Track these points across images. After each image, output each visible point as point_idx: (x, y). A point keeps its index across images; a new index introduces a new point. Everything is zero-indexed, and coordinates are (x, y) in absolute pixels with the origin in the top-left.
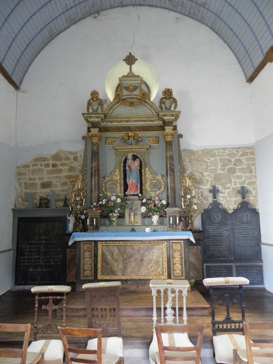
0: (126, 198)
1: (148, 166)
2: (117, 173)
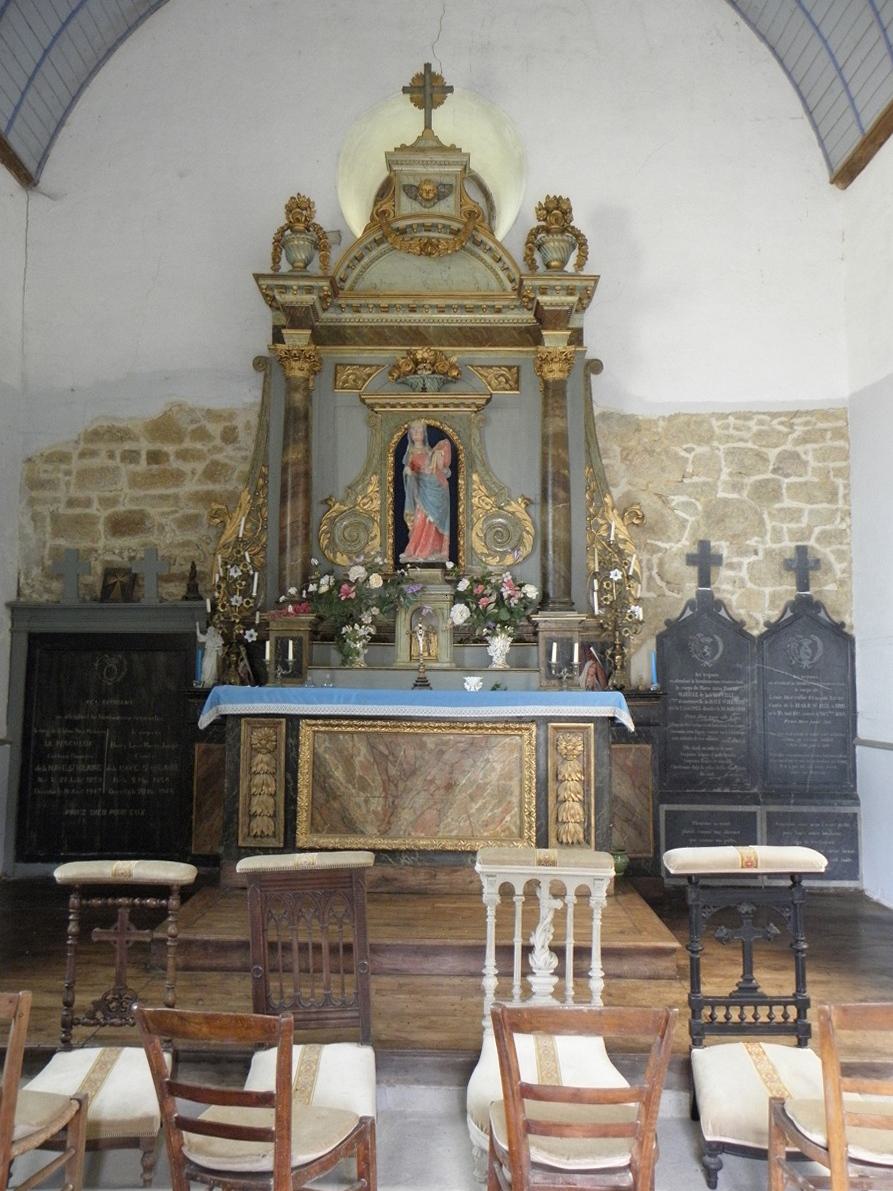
2: (370, 488)
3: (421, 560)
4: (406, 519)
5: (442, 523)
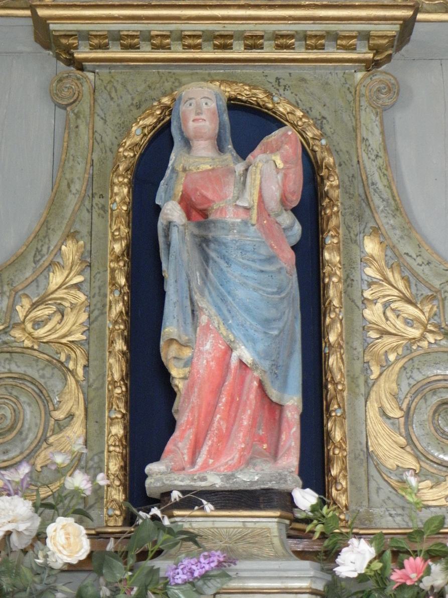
0: (155, 518)
1: (385, 221)
2: (56, 279)
3: (215, 481)
4: (169, 354)
5: (279, 371)
